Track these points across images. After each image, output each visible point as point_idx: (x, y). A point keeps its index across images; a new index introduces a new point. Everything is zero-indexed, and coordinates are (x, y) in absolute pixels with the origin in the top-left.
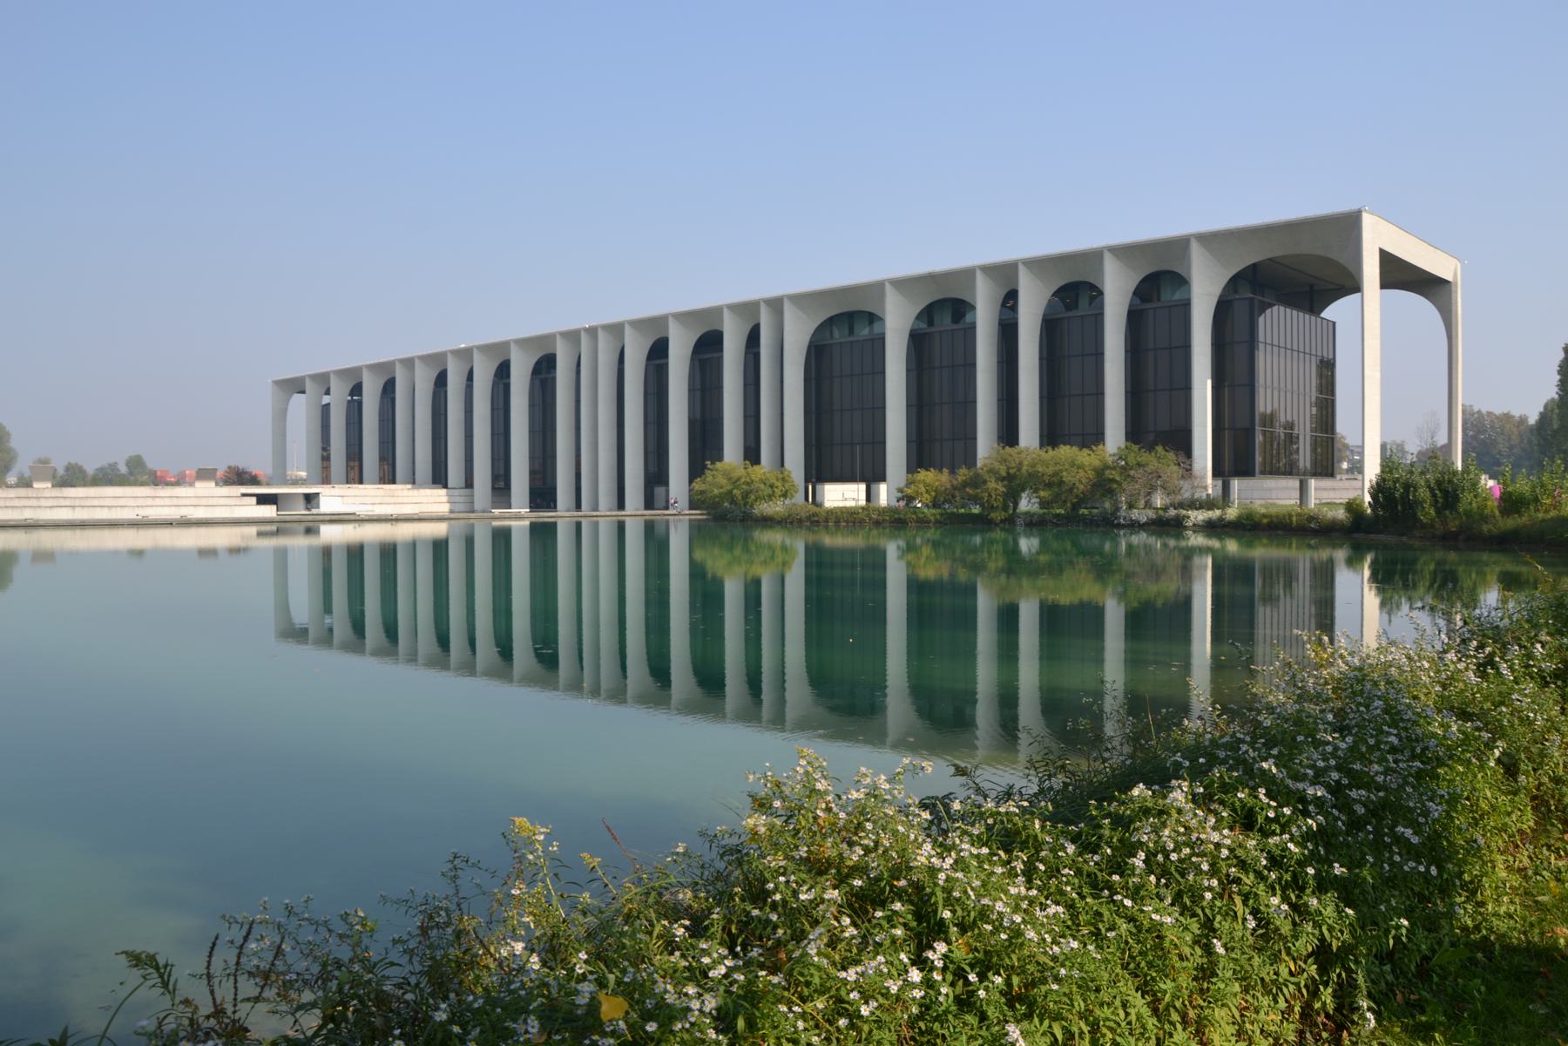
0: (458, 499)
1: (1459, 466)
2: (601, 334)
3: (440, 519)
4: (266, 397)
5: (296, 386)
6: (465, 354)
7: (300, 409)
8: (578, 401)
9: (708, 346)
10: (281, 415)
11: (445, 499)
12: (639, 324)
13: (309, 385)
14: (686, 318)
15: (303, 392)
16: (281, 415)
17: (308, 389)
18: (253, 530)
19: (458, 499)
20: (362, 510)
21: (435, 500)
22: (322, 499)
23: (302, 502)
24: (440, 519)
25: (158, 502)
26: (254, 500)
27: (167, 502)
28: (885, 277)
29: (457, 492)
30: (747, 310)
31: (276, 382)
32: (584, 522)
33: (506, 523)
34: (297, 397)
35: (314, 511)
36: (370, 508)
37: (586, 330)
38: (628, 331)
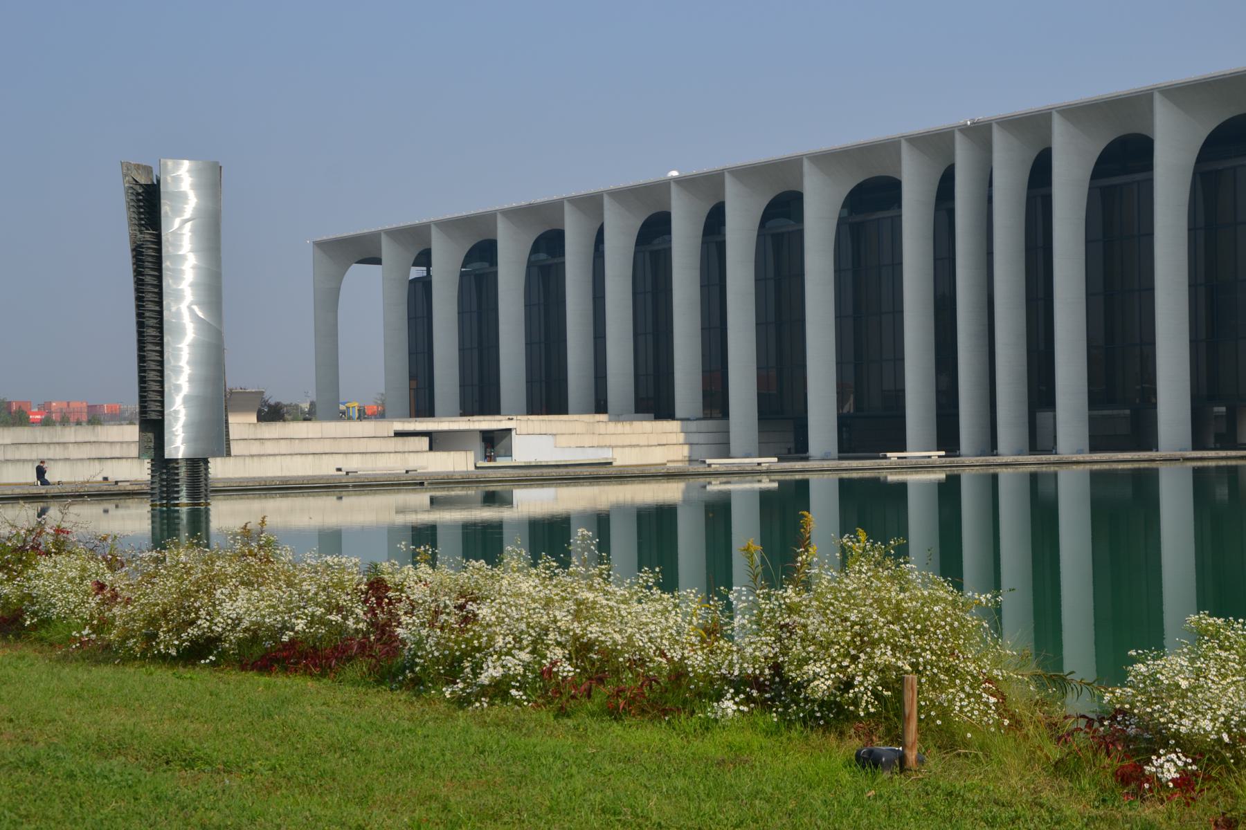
0: (696, 438)
1: (1128, 412)
2: (998, 137)
3: (670, 476)
4: (301, 274)
5: (364, 251)
6: (591, 204)
7: (371, 296)
8: (990, 254)
9: (871, 201)
10: (328, 301)
11: (681, 438)
12: (625, 196)
13: (388, 250)
14: (750, 174)
15: (378, 261)
16: (328, 301)
17: (385, 257)
18: (423, 498)
19: (696, 438)
20: (623, 459)
21: (659, 443)
22: (517, 442)
23: (478, 444)
24: (670, 476)
25: (270, 448)
26: (425, 441)
27: (283, 447)
28: (602, 189)
29: (693, 426)
30: (936, 144)
31: (323, 246)
32: (966, 478)
33: (806, 476)
34: (358, 272)
35: (501, 462)
36: (340, 461)
37: (965, 130)
38: (609, 206)
